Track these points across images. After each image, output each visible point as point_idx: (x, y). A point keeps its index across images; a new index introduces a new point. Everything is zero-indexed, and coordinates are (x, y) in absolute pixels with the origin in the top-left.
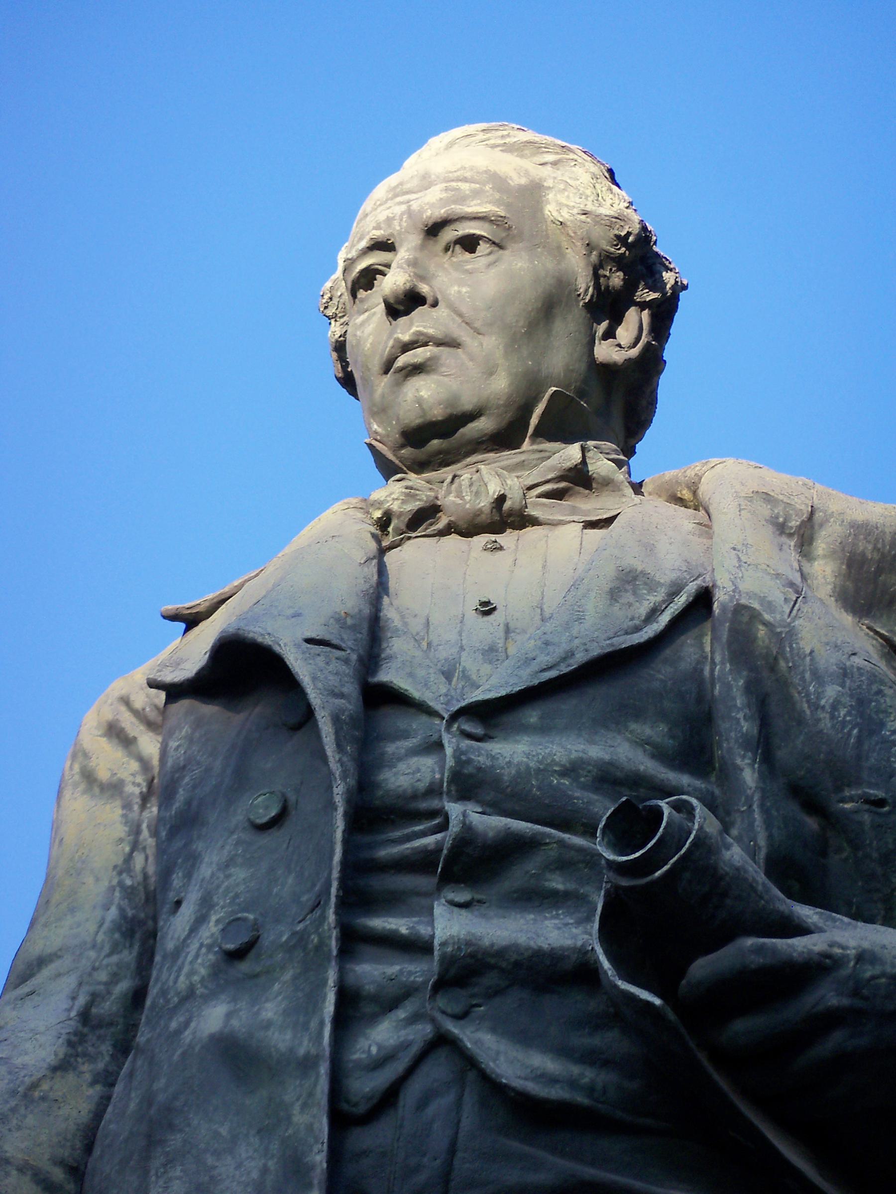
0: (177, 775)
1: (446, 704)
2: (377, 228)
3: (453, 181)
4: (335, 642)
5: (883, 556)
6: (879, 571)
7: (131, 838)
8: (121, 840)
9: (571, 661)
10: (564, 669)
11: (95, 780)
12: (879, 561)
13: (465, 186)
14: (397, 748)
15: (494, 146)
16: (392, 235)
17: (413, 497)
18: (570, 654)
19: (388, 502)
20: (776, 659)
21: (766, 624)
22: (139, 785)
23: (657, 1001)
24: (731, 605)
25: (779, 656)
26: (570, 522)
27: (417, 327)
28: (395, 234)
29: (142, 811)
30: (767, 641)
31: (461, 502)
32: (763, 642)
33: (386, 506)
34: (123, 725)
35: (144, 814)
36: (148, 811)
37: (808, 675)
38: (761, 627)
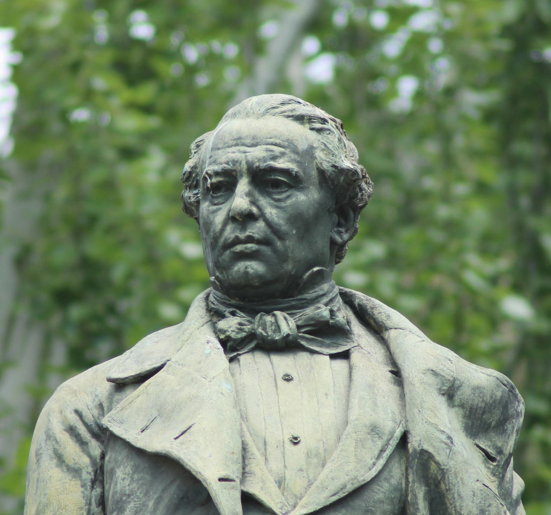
0: (124, 498)
1: (281, 509)
3: (269, 144)
5: (486, 404)
6: (484, 413)
7: (87, 507)
8: (81, 508)
9: (345, 490)
10: (342, 495)
11: (64, 462)
12: (485, 407)
13: (277, 150)
15: (288, 117)
16: (235, 171)
17: (241, 330)
18: (344, 487)
20: (439, 482)
21: (437, 463)
22: (90, 474)
24: (418, 449)
25: (442, 481)
27: (250, 232)
28: (238, 170)
29: (92, 491)
30: (436, 472)
32: (434, 471)
33: (228, 334)
34: (80, 432)
35: (93, 492)
36: (94, 490)
37: (456, 495)
38: (433, 463)
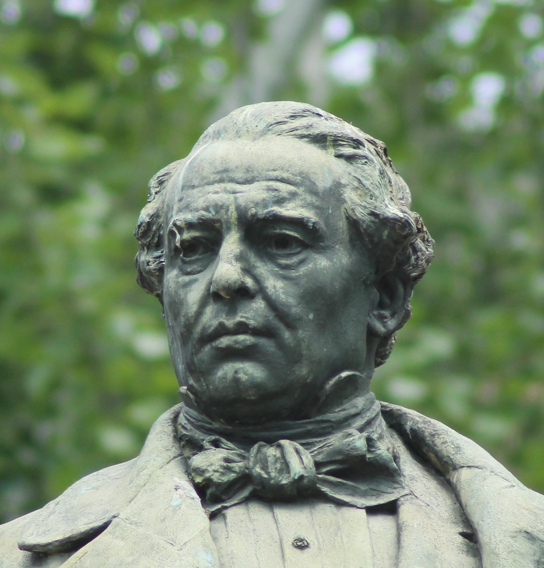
2: (207, 209)
3: (272, 180)
4: (278, 543)
14: (412, 479)
16: (219, 221)
19: (209, 472)
23: (413, 292)
26: (231, 506)
27: (242, 317)
28: (223, 221)
31: (265, 476)
33: (207, 475)
